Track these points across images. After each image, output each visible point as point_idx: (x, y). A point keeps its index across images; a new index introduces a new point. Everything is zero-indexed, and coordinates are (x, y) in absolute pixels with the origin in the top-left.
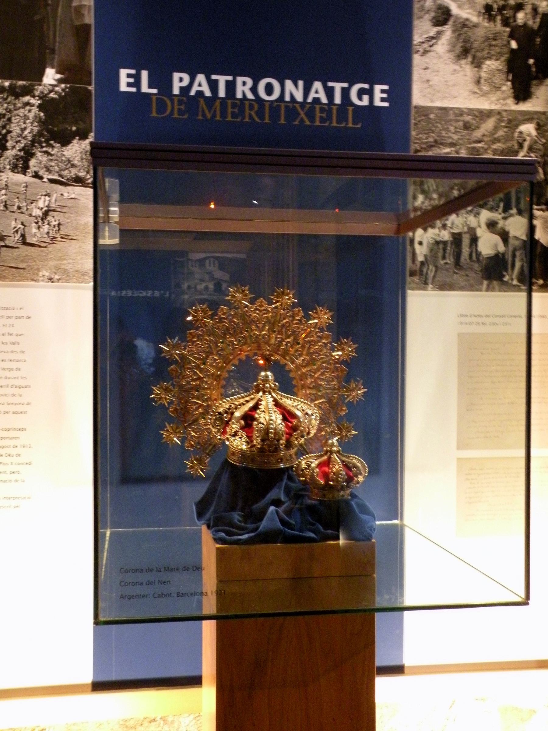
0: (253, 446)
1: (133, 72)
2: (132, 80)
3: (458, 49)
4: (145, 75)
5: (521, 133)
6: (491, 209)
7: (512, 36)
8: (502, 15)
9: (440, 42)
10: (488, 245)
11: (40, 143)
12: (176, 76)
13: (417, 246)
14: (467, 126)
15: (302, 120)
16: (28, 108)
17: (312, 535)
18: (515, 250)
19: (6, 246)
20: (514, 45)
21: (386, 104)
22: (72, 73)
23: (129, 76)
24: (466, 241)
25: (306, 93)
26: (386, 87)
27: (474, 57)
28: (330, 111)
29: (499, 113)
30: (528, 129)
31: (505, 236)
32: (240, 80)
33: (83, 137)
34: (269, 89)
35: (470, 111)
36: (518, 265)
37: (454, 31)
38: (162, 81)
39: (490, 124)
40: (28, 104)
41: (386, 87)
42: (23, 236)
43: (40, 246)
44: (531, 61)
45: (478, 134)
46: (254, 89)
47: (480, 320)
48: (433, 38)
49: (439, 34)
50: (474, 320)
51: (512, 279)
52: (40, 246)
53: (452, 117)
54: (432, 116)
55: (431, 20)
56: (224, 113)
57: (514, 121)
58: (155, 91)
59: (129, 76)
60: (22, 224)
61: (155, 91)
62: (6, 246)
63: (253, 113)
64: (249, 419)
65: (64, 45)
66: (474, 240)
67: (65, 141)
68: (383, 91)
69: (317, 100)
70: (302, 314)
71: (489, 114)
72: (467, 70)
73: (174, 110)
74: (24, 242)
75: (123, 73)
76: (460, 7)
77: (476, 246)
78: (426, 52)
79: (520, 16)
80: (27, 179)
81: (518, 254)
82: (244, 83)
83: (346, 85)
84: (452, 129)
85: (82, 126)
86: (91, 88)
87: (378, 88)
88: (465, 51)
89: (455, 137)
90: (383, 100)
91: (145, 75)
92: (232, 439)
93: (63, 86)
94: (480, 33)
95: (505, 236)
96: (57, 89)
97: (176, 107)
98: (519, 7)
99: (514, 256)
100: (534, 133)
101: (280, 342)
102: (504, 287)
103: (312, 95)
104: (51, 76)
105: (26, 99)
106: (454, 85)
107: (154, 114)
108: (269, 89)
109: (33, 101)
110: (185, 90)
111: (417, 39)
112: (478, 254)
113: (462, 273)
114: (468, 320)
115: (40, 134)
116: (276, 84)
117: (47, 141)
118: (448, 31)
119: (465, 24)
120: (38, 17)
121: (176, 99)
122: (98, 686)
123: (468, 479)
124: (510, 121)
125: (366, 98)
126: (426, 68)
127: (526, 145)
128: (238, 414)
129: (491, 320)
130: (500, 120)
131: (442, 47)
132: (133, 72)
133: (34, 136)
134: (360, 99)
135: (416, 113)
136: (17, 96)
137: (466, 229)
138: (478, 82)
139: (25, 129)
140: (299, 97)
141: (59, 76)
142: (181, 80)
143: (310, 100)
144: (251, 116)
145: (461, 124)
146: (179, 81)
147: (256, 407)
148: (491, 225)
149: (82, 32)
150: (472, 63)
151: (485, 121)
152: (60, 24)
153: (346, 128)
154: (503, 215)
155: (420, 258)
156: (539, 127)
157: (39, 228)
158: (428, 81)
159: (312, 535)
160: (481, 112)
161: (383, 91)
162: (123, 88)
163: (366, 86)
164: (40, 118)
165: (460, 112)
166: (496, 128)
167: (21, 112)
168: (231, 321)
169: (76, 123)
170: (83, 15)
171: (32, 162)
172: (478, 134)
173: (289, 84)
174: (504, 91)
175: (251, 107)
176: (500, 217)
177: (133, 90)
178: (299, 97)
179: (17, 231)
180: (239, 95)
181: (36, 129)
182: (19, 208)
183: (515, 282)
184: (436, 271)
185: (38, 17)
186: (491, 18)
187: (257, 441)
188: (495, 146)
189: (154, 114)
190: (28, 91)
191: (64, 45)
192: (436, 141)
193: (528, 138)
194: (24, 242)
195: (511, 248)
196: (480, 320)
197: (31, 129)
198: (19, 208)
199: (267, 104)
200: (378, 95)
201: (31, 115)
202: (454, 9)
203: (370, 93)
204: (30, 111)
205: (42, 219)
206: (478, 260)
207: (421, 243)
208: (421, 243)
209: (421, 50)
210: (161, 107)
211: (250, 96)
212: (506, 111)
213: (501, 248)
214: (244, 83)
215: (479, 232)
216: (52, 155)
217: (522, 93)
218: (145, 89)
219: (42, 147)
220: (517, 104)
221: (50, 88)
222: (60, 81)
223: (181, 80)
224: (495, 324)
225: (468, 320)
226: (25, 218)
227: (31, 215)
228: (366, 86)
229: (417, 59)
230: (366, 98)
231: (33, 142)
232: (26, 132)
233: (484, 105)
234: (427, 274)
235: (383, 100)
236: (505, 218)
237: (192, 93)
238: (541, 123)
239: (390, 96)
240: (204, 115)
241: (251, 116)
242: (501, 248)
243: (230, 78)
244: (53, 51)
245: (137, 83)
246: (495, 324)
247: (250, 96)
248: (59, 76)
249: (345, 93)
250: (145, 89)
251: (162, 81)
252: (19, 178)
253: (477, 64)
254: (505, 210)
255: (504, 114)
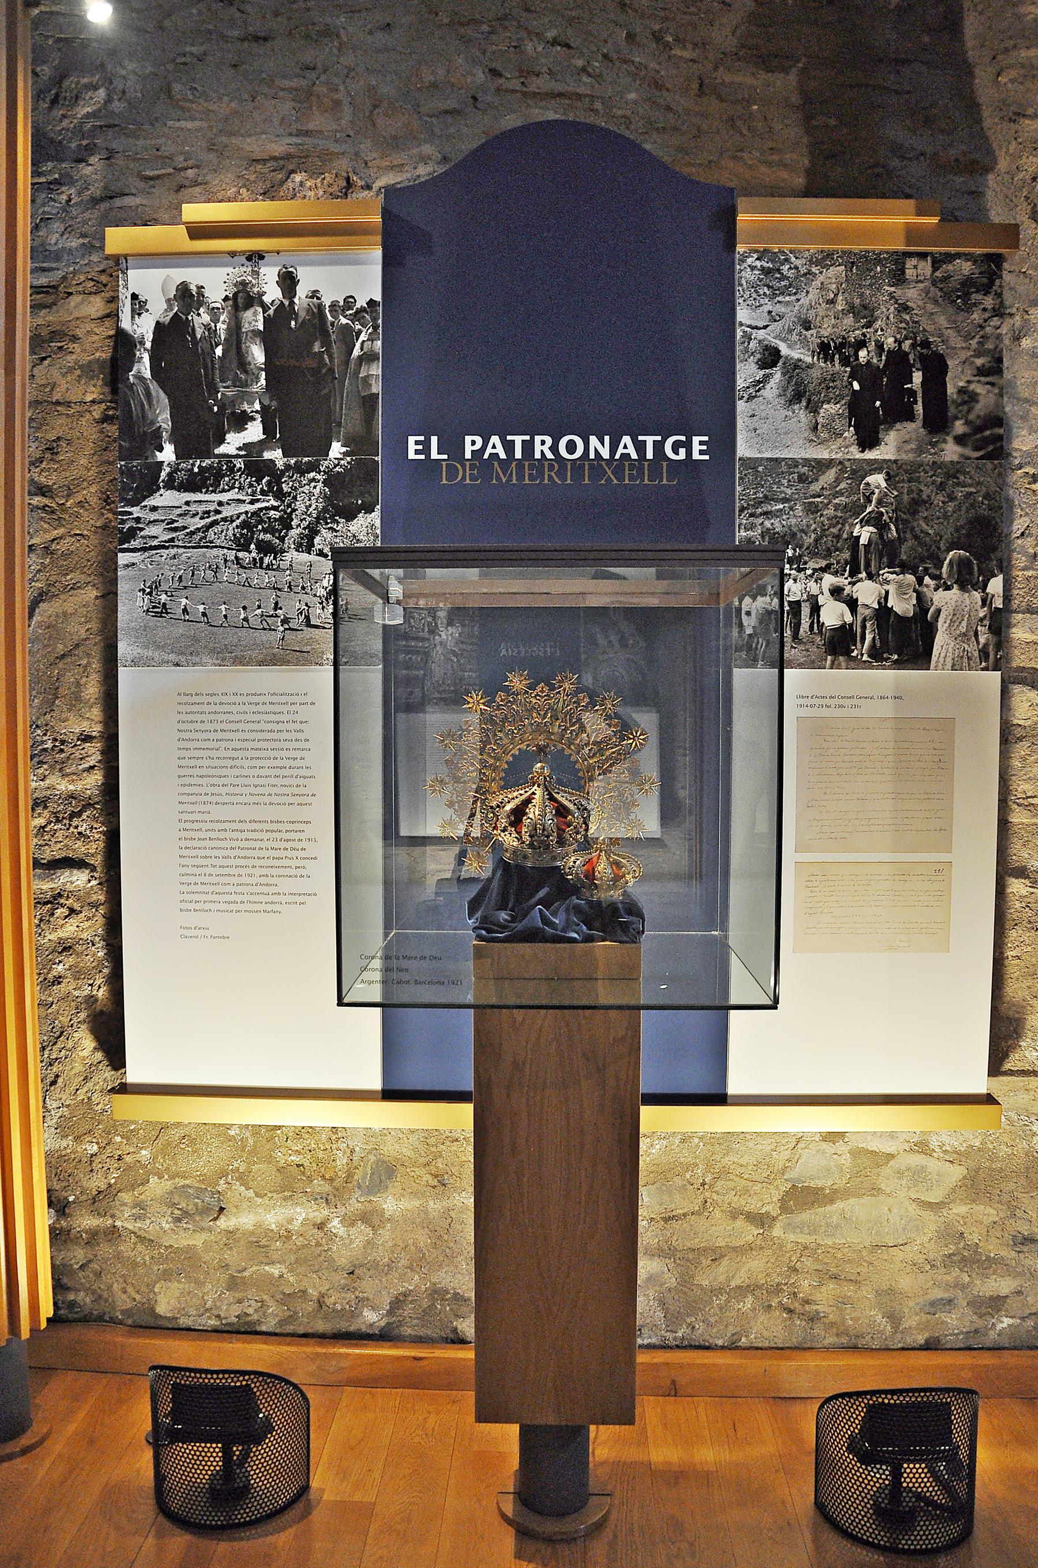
0: (523, 843)
1: (422, 438)
2: (420, 447)
3: (789, 393)
4: (434, 440)
5: (868, 484)
6: (835, 573)
7: (853, 376)
8: (841, 354)
9: (768, 387)
10: (833, 614)
11: (325, 519)
12: (468, 439)
13: (743, 616)
14: (802, 479)
15: (609, 479)
16: (313, 484)
17: (576, 935)
18: (864, 620)
19: (290, 629)
20: (856, 386)
21: (707, 457)
22: (360, 444)
23: (417, 443)
24: (806, 610)
25: (613, 450)
26: (706, 438)
27: (809, 401)
28: (641, 469)
29: (840, 463)
30: (878, 480)
31: (852, 604)
32: (538, 439)
33: (370, 510)
34: (571, 447)
35: (806, 462)
36: (869, 637)
37: (784, 374)
38: (453, 446)
39: (831, 475)
40: (313, 480)
41: (706, 438)
42: (307, 618)
43: (324, 628)
44: (878, 403)
45: (816, 487)
46: (554, 449)
47: (824, 702)
48: (759, 382)
49: (766, 379)
50: (815, 701)
51: (862, 655)
52: (324, 628)
53: (784, 469)
54: (760, 469)
55: (757, 363)
56: (521, 477)
57: (859, 472)
58: (445, 457)
59: (417, 443)
60: (306, 605)
61: (445, 457)
62: (290, 629)
63: (553, 474)
64: (519, 813)
65: (350, 418)
66: (816, 609)
67: (350, 517)
68: (701, 443)
69: (626, 456)
70: (587, 700)
71: (829, 464)
72: (801, 415)
73: (465, 476)
74: (309, 624)
75: (412, 440)
76: (789, 347)
77: (819, 616)
78: (751, 398)
79: (863, 354)
80: (313, 558)
81: (868, 624)
82: (543, 443)
83: (659, 438)
84: (785, 482)
85: (368, 498)
86: (379, 459)
87: (696, 440)
88: (798, 393)
89: (789, 491)
90: (701, 452)
91: (434, 440)
92: (502, 834)
93: (349, 459)
94: (816, 373)
95: (852, 604)
96: (342, 462)
97: (468, 472)
98: (861, 344)
99: (864, 627)
100: (884, 484)
101: (565, 730)
102: (852, 664)
103: (621, 450)
104: (336, 449)
105: (312, 475)
106: (786, 433)
107: (444, 482)
108: (571, 447)
109: (318, 477)
110: (477, 454)
111: (740, 383)
112: (821, 626)
113: (802, 647)
114: (809, 701)
115: (325, 510)
116: (578, 441)
117: (332, 517)
118: (777, 375)
119: (797, 365)
120: (326, 391)
121: (468, 464)
122: (389, 1094)
123: (808, 887)
124: (854, 472)
125: (682, 452)
126: (753, 416)
127: (875, 498)
128: (508, 807)
129: (837, 701)
130: (843, 471)
131: (771, 391)
132: (422, 438)
133: (319, 513)
134: (677, 454)
135: (741, 465)
136: (303, 473)
137: (805, 597)
138: (815, 428)
139: (310, 506)
140: (605, 454)
141: (344, 449)
142: (473, 443)
143: (617, 457)
144: (550, 477)
145: (796, 476)
146: (471, 444)
147: (528, 801)
148: (836, 592)
149: (369, 402)
150: (807, 407)
151: (824, 473)
152: (347, 396)
153: (660, 486)
154: (850, 579)
155: (749, 631)
156: (889, 478)
157: (323, 608)
158: (755, 430)
159: (576, 935)
160: (818, 462)
161: (701, 443)
162: (411, 455)
163: (683, 438)
164: (325, 494)
165: (794, 463)
166: (838, 481)
167: (306, 489)
168: (510, 708)
169: (361, 495)
170: (371, 385)
171: (317, 540)
172: (816, 487)
173: (593, 440)
174: (845, 438)
175: (551, 467)
176: (846, 582)
177: (422, 457)
178: (605, 454)
179: (301, 613)
180: (538, 456)
181: (320, 506)
182: (303, 588)
183: (865, 658)
184: (767, 646)
185: (326, 391)
186: (828, 357)
187: (526, 838)
188: (837, 501)
189: (444, 482)
190: (314, 467)
191: (350, 418)
192: (766, 497)
193: (877, 491)
194: (309, 624)
195: (860, 619)
196: (824, 702)
197: (317, 505)
198: (303, 588)
199: (569, 464)
200: (696, 447)
201: (317, 491)
202: (784, 350)
203: (688, 445)
204: (315, 487)
205: (327, 599)
206: (820, 632)
207: (748, 613)
208: (748, 613)
209: (746, 396)
210: (452, 472)
211: (550, 455)
212: (849, 460)
213: (848, 618)
214: (543, 443)
215: (821, 600)
216: (337, 531)
217: (868, 440)
218: (435, 455)
219: (327, 523)
220: (863, 451)
221: (336, 462)
222: (345, 454)
223: (473, 443)
224: (841, 706)
225: (809, 701)
226: (306, 598)
227: (315, 595)
228: (683, 438)
229: (741, 406)
230: (682, 452)
231: (318, 518)
232: (311, 510)
233: (823, 454)
234: (756, 648)
235: (701, 452)
236: (853, 584)
237: (486, 456)
238: (892, 473)
239: (710, 448)
240: (498, 478)
241: (550, 477)
242: (848, 618)
243: (528, 438)
244: (339, 424)
245: (426, 450)
246: (841, 706)
247: (550, 455)
248: (344, 449)
249: (659, 447)
250: (435, 455)
251: (453, 446)
252: (304, 557)
253: (813, 408)
254: (852, 574)
255: (847, 464)
